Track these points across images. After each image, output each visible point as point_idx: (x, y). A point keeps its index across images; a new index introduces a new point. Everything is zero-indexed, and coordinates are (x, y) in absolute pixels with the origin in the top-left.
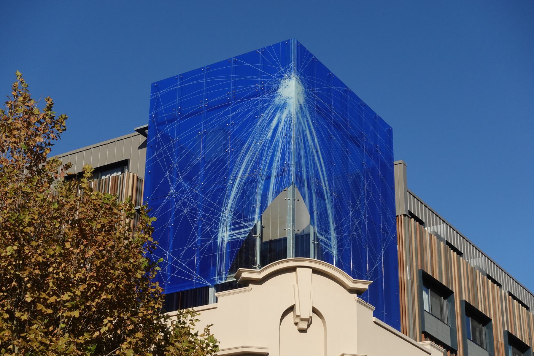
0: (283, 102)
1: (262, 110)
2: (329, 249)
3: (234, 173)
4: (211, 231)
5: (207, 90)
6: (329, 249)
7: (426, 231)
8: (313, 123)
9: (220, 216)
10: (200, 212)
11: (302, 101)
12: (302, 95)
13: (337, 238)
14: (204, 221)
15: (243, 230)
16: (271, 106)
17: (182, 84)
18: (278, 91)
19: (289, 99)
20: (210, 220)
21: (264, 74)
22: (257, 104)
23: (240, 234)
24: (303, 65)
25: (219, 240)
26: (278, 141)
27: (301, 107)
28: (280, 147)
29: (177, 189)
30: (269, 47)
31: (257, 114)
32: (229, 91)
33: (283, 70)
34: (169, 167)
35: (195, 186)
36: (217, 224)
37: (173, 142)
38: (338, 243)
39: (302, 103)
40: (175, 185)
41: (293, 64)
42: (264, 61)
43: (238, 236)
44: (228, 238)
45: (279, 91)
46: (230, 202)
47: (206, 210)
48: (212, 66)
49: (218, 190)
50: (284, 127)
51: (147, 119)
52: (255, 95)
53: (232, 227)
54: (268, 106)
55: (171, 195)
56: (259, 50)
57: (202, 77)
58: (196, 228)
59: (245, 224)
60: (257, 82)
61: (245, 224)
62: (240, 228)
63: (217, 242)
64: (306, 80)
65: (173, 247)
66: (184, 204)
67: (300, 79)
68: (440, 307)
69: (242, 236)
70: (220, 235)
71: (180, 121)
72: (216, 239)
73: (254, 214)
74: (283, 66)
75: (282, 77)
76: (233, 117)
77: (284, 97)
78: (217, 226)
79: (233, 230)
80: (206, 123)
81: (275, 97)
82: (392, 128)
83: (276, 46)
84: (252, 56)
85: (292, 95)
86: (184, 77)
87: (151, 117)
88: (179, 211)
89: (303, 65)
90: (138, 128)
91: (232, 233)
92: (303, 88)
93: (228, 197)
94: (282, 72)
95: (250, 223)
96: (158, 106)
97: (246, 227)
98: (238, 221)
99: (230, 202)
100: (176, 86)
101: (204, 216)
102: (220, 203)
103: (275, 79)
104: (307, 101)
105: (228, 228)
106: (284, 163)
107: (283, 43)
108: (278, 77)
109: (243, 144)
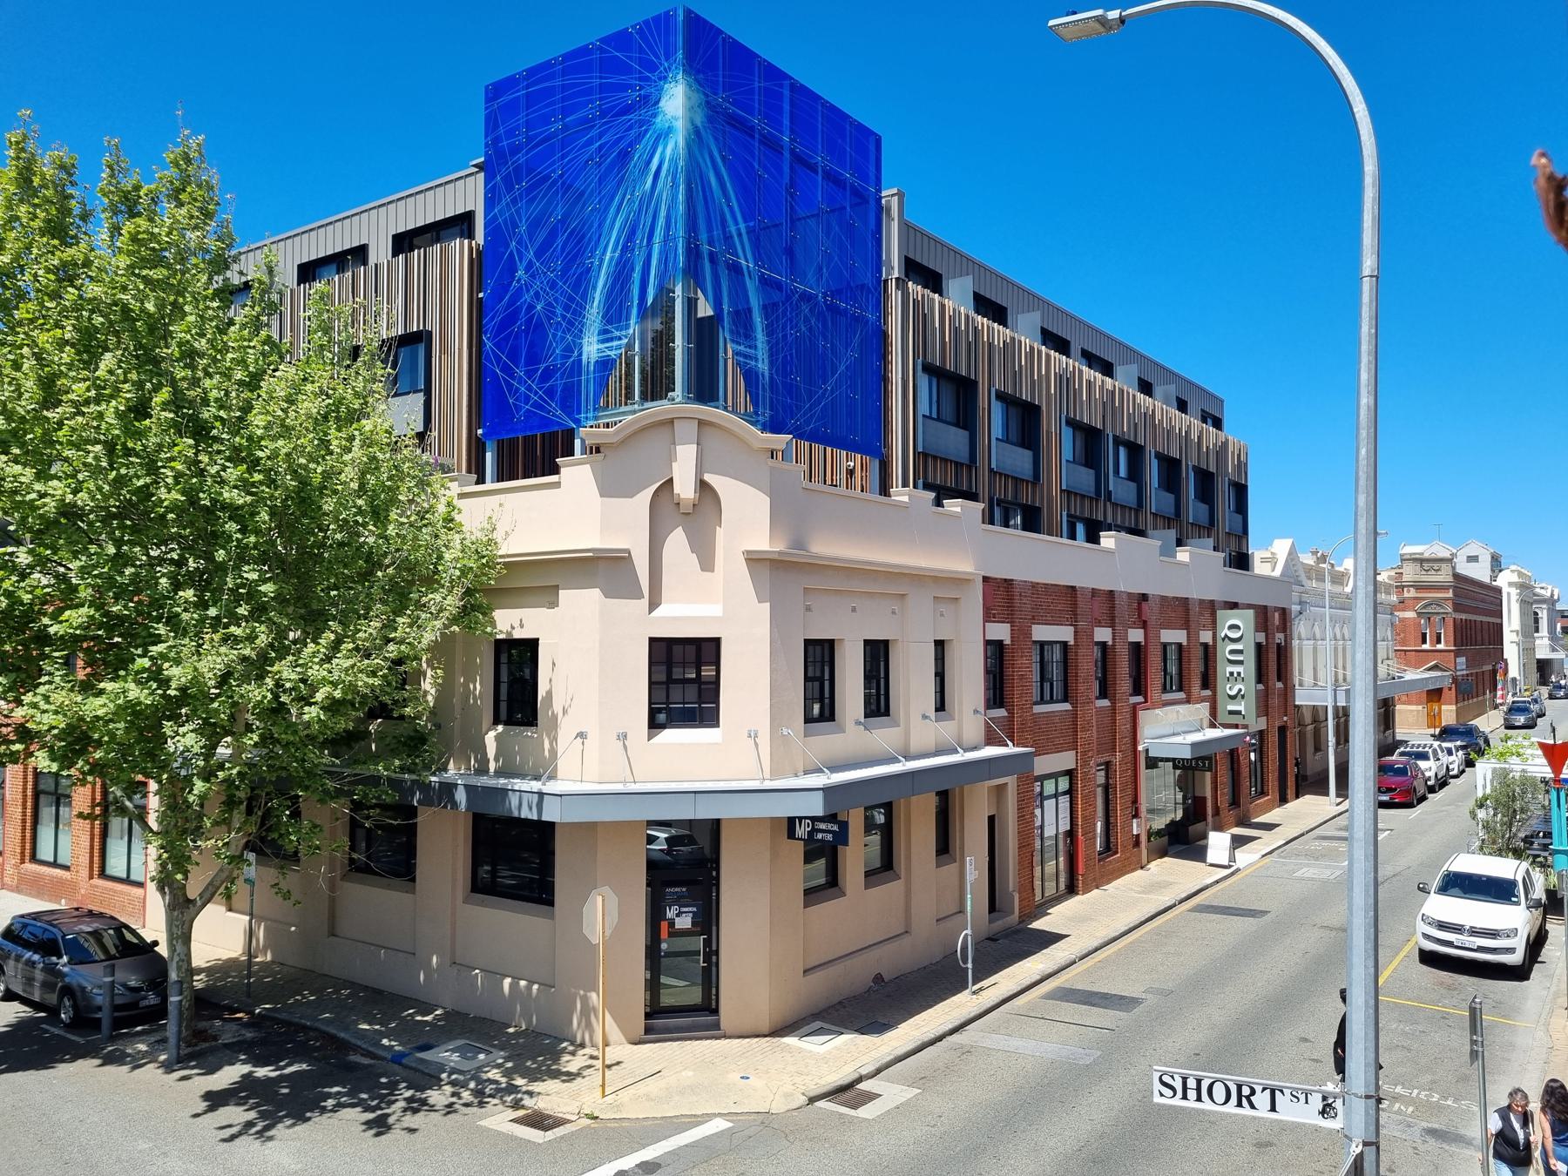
0: (667, 125)
1: (640, 137)
2: (753, 363)
3: (602, 246)
4: (574, 342)
5: (563, 99)
6: (753, 363)
7: (235, 1055)
8: (723, 158)
9: (584, 317)
10: (559, 311)
11: (699, 120)
12: (699, 110)
13: (768, 342)
14: (564, 324)
15: (615, 343)
16: (650, 132)
17: (528, 87)
18: (661, 104)
19: (676, 119)
20: (571, 323)
21: (640, 72)
22: (630, 128)
23: (610, 348)
24: (701, 52)
25: (584, 358)
26: (660, 195)
27: (697, 132)
28: (663, 206)
29: (527, 270)
30: (646, 22)
31: (631, 145)
32: (592, 102)
33: (666, 65)
34: (514, 233)
35: (550, 267)
36: (581, 331)
37: (518, 189)
38: (771, 349)
39: (699, 124)
40: (525, 263)
41: (680, 55)
42: (641, 50)
43: (609, 353)
44: (596, 355)
45: (662, 104)
46: (598, 296)
47: (567, 308)
48: (567, 57)
49: (581, 274)
50: (668, 171)
51: (482, 149)
52: (627, 110)
53: (601, 337)
54: (646, 131)
55: (519, 280)
56: (632, 27)
57: (552, 77)
58: (555, 336)
59: (618, 334)
60: (632, 87)
61: (618, 334)
62: (612, 340)
63: (581, 360)
64: (707, 80)
65: (527, 364)
66: (537, 295)
67: (696, 80)
68: (895, 1058)
69: (614, 352)
70: (586, 349)
71: (527, 153)
72: (580, 355)
73: (628, 319)
74: (667, 59)
75: (665, 78)
76: (601, 147)
77: (669, 117)
78: (579, 335)
79: (603, 342)
80: (563, 157)
81: (655, 115)
82: (880, 137)
83: (656, 19)
84: (620, 39)
85: (680, 112)
86: (532, 72)
87: (487, 145)
88: (531, 307)
89: (701, 52)
90: (474, 162)
91: (602, 346)
92: (702, 97)
93: (594, 288)
94: (665, 69)
95: (624, 333)
96: (496, 126)
97: (620, 339)
98: (609, 327)
99: (598, 296)
100: (518, 91)
101: (564, 317)
102: (584, 297)
103: (655, 82)
104: (710, 120)
105: (596, 339)
106: (668, 235)
107: (667, 13)
108: (660, 79)
109: (612, 199)
